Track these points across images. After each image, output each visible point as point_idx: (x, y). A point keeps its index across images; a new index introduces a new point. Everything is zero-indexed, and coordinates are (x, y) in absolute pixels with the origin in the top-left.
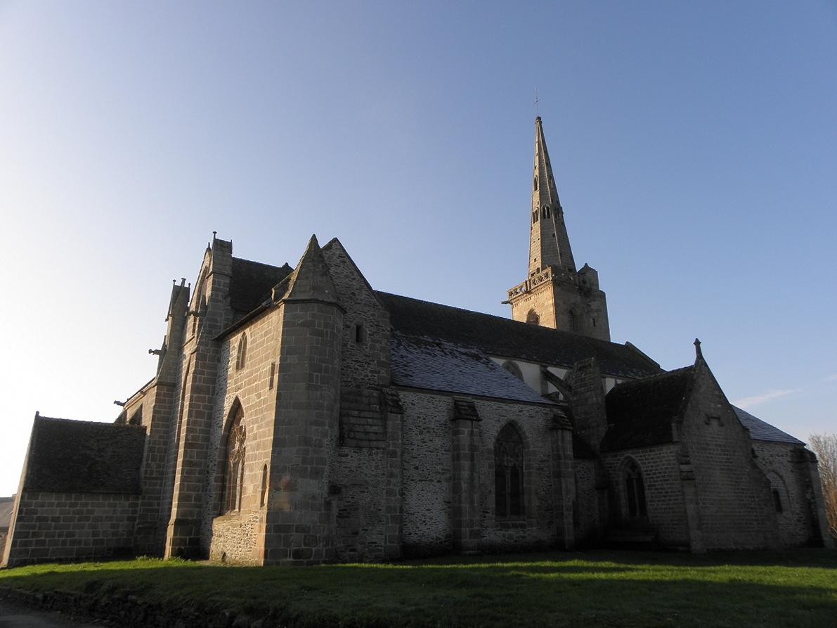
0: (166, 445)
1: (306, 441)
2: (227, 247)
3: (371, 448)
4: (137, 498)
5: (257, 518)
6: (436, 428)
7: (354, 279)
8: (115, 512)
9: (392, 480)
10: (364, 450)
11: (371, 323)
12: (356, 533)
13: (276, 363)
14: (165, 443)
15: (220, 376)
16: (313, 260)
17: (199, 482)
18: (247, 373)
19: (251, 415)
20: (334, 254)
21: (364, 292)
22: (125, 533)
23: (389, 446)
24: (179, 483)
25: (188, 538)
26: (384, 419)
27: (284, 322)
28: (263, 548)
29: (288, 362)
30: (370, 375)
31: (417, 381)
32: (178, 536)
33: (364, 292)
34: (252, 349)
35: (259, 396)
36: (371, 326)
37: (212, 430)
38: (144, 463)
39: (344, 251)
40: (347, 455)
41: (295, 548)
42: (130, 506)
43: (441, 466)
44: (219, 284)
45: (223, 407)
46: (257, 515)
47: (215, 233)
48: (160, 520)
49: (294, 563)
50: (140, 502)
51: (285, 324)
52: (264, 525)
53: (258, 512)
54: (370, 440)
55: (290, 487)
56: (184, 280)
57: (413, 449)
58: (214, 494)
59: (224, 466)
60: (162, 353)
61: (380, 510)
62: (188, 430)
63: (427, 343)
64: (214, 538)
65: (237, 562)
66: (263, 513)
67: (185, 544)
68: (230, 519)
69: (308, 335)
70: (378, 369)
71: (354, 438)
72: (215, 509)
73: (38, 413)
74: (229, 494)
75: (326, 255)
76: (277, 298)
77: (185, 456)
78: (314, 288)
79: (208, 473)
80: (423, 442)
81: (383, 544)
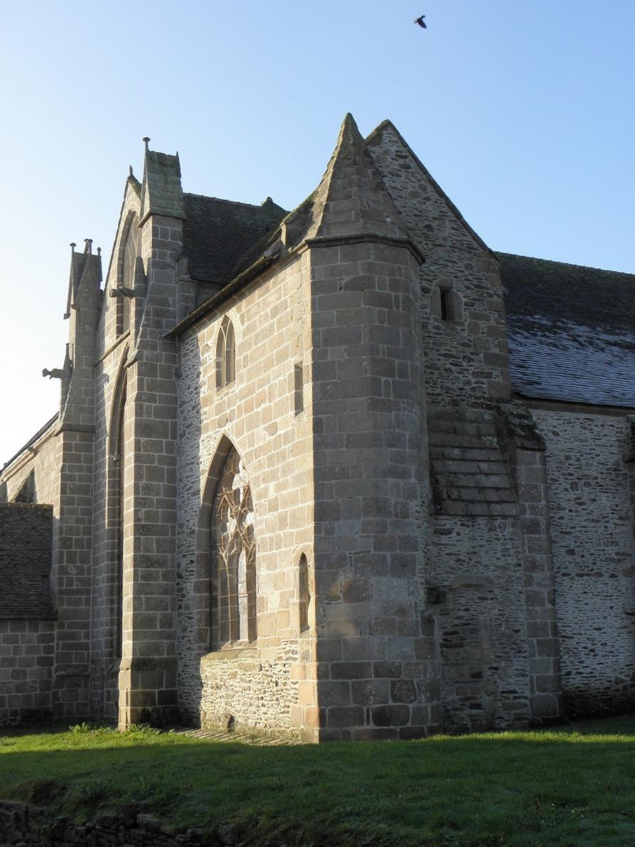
0: (90, 533)
1: (379, 507)
2: (172, 166)
3: (492, 517)
4: (51, 627)
5: (294, 652)
6: (600, 476)
7: (428, 199)
8: (16, 650)
9: (534, 575)
10: (481, 521)
11: (467, 283)
12: (477, 676)
13: (305, 364)
14: (88, 531)
15: (184, 403)
16: (355, 163)
17: (165, 592)
18: (241, 390)
19: (260, 466)
20: (387, 152)
21: (447, 223)
22: (37, 685)
23: (523, 511)
24: (131, 596)
25: (156, 691)
26: (511, 462)
27: (313, 284)
28: (314, 706)
29: (329, 359)
30: (473, 380)
31: (554, 392)
32: (140, 690)
33: (447, 223)
34: (246, 345)
35: (273, 429)
36: (467, 288)
37: (179, 501)
38: (55, 566)
39: (405, 145)
40: (450, 532)
41: (377, 705)
42: (42, 639)
43: (616, 549)
44: (164, 234)
45: (196, 457)
46: (293, 647)
47: (147, 140)
48: (93, 662)
49: (377, 735)
50: (55, 633)
51: (316, 287)
52: (312, 666)
53: (296, 642)
54: (488, 502)
55: (355, 594)
56: (89, 242)
57: (562, 518)
58: (197, 612)
59: (210, 562)
60: (65, 374)
61: (517, 631)
62: (138, 503)
63: (542, 328)
64: (207, 691)
65: (259, 732)
66: (309, 642)
67: (153, 703)
68: (236, 657)
69: (363, 306)
70: (488, 369)
71: (459, 499)
72: (201, 638)
73: (423, 17)
74: (225, 611)
75: (376, 151)
76: (292, 240)
77: (137, 548)
78: (364, 214)
79: (180, 576)
80: (580, 504)
81: (527, 693)
